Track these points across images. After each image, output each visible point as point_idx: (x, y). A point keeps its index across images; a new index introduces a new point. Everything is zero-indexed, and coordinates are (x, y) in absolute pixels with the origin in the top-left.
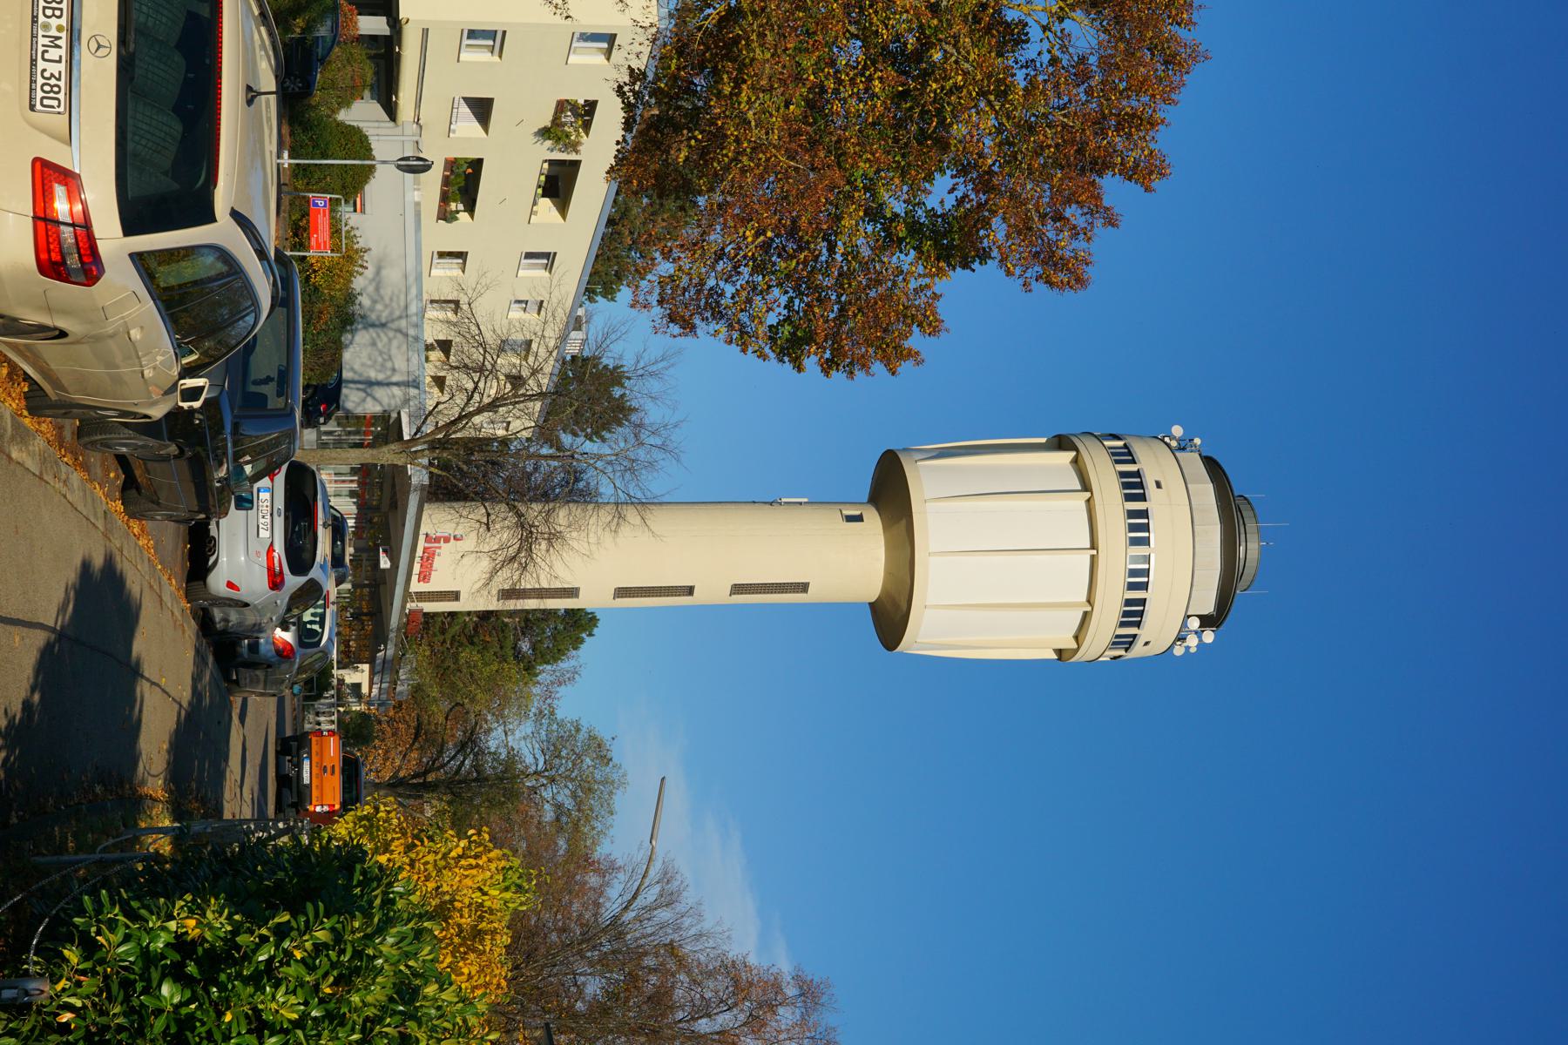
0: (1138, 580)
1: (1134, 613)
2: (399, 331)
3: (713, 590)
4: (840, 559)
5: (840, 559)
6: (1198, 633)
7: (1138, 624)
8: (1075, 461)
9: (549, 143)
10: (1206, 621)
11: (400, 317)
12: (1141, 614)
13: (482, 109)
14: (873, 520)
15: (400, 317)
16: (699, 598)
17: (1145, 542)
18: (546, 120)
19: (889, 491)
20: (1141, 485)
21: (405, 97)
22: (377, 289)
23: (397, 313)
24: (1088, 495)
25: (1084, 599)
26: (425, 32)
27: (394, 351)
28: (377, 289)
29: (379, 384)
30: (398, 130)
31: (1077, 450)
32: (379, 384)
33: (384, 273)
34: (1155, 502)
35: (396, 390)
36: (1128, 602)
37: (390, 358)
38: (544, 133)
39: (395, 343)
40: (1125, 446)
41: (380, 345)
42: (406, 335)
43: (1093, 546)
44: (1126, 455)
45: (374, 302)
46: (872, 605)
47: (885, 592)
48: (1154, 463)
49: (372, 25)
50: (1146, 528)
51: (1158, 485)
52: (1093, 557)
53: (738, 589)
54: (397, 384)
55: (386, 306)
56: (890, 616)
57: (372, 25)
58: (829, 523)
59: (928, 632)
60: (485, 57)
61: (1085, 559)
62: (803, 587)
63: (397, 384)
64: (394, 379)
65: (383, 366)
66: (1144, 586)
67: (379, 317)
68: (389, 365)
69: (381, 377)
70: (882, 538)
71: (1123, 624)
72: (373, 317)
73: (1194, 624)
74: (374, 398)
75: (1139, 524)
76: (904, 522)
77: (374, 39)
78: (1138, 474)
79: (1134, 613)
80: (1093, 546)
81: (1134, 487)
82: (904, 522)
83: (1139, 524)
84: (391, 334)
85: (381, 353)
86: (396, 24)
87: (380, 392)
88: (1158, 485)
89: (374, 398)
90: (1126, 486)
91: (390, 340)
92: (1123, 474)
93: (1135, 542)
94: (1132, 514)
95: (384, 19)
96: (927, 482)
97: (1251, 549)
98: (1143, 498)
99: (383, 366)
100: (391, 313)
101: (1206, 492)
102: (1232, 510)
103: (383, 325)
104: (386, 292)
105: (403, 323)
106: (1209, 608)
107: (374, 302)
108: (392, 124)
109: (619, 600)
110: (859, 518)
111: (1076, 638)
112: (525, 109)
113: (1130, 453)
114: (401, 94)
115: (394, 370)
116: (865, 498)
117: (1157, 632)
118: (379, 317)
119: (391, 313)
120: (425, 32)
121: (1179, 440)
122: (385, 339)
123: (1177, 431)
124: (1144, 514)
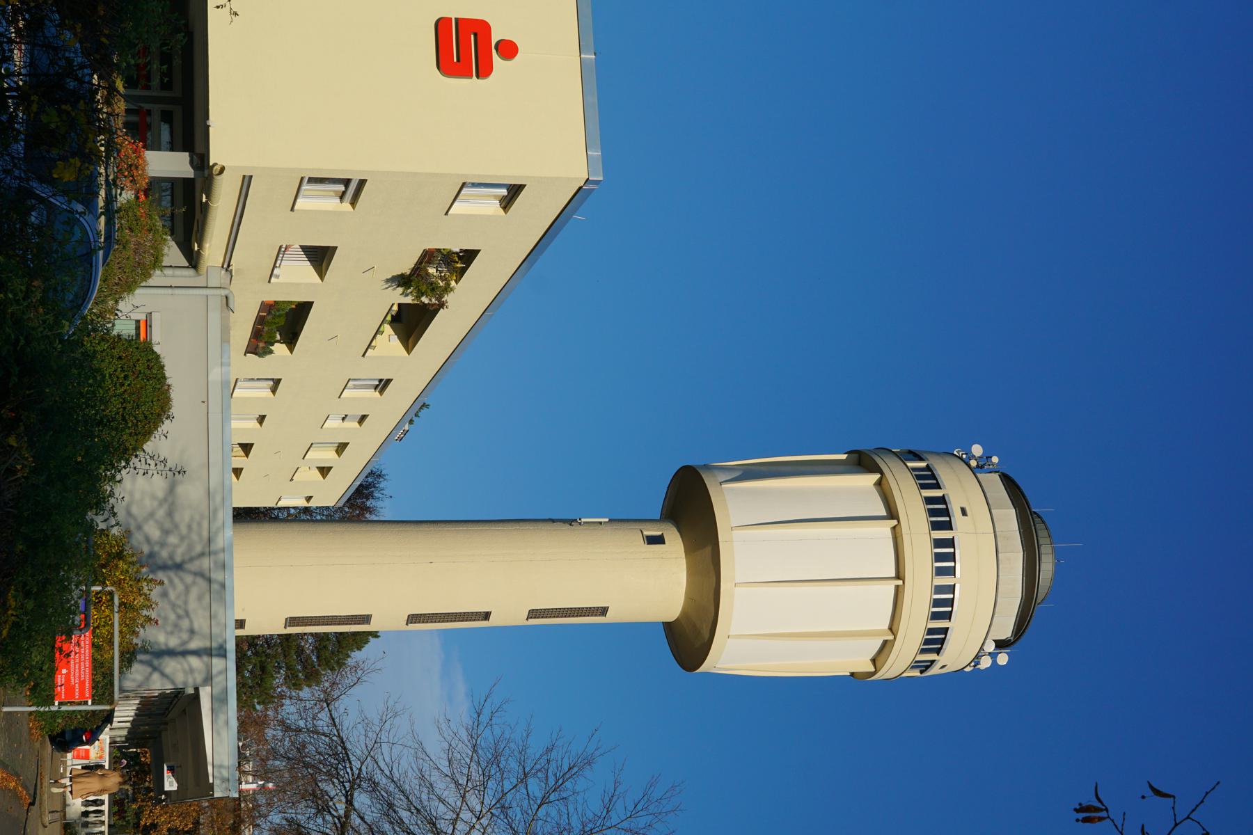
0: (943, 607)
1: (935, 641)
2: (200, 574)
3: (509, 611)
4: (641, 581)
5: (641, 581)
6: (993, 656)
7: (938, 651)
8: (879, 484)
9: (400, 290)
10: (1000, 644)
11: (202, 555)
12: (942, 641)
13: (320, 257)
14: (675, 544)
15: (202, 555)
16: (493, 621)
17: (951, 572)
18: (406, 267)
19: (687, 509)
20: (946, 512)
21: (213, 249)
22: (170, 514)
23: (198, 549)
24: (894, 522)
25: (886, 626)
26: (247, 181)
27: (193, 605)
28: (170, 514)
29: (171, 653)
30: (200, 281)
31: (882, 473)
32: (171, 653)
33: (180, 489)
34: (962, 530)
35: (194, 661)
36: (931, 631)
37: (187, 614)
38: (403, 281)
39: (194, 592)
40: (928, 468)
41: (172, 595)
42: (210, 581)
43: (899, 576)
44: (928, 479)
45: (166, 532)
46: (668, 627)
47: (684, 613)
48: (959, 487)
49: (166, 163)
50: (952, 557)
51: (964, 512)
52: (897, 587)
53: (534, 614)
54: (196, 653)
55: (182, 538)
56: (688, 639)
57: (166, 163)
58: (630, 543)
59: (730, 655)
60: (332, 204)
61: (889, 588)
62: (603, 611)
63: (196, 653)
64: (194, 645)
65: (176, 626)
66: (948, 616)
67: (171, 557)
68: (185, 624)
69: (173, 642)
70: (684, 561)
71: (923, 651)
72: (164, 554)
73: (990, 647)
74: (163, 675)
75: (945, 553)
76: (708, 549)
77: (174, 184)
78: (942, 500)
79: (935, 641)
80: (899, 576)
81: (940, 514)
82: (708, 549)
83: (945, 553)
84: (189, 579)
85: (174, 606)
86: (201, 161)
87: (171, 666)
88: (964, 512)
89: (163, 675)
90: (932, 513)
91: (187, 589)
92: (929, 500)
93: (940, 572)
94: (938, 543)
95: (187, 154)
96: (733, 504)
97: (1047, 568)
98: (948, 526)
99: (176, 626)
100: (190, 547)
101: (1008, 517)
102: (1030, 525)
103: (179, 567)
104: (183, 517)
105: (205, 563)
106: (1006, 632)
107: (166, 532)
108: (191, 272)
109: (659, 533)
110: (658, 540)
111: (874, 661)
112: (379, 250)
113: (933, 477)
114: (207, 246)
115: (192, 632)
116: (655, 506)
117: (955, 656)
118: (171, 557)
119: (190, 547)
120: (247, 181)
121: (978, 459)
122: (180, 587)
123: (977, 450)
124: (950, 543)
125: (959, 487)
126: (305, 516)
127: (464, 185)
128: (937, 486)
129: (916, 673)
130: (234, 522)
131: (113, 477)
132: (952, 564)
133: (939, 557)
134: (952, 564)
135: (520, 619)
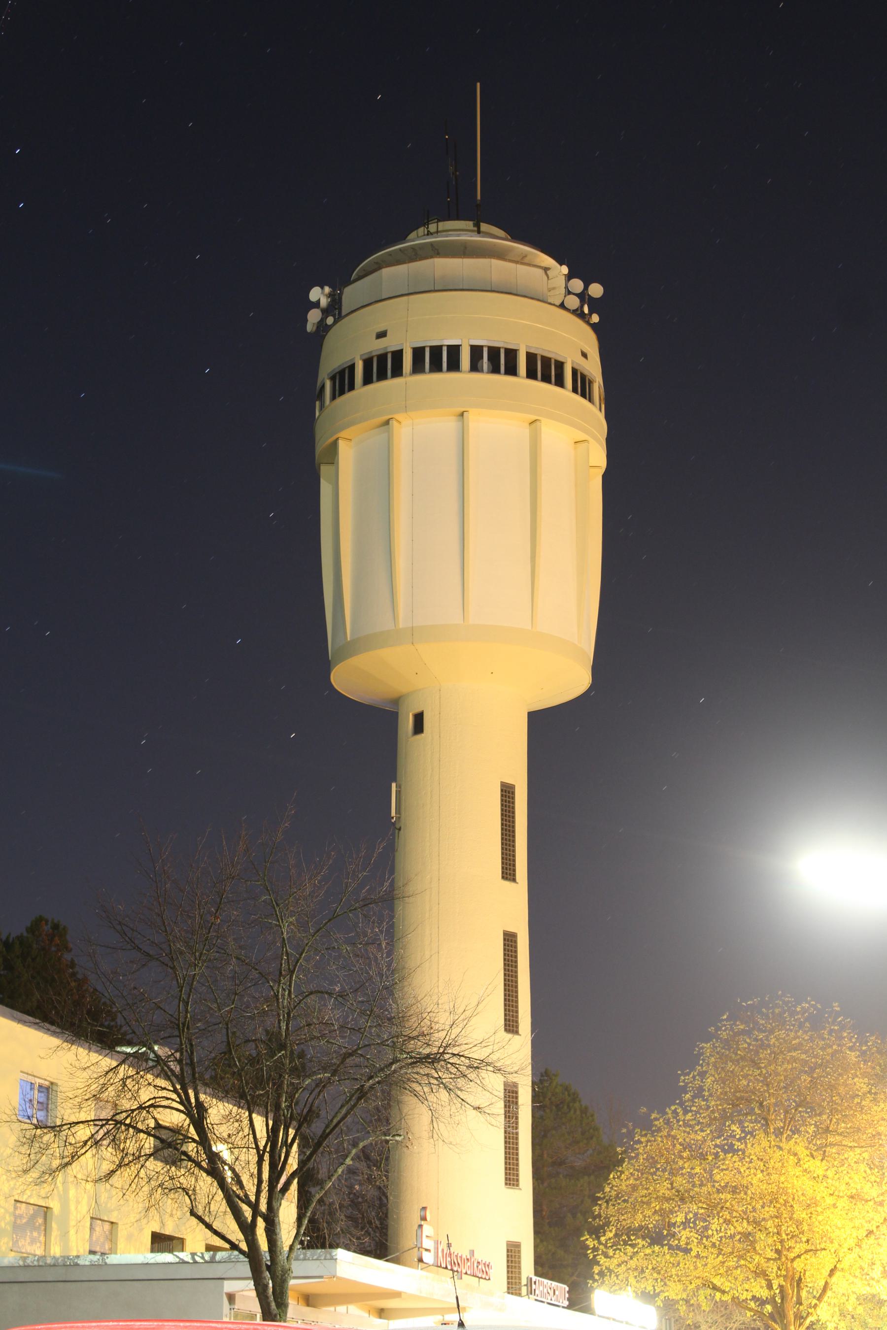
20: (382, 358)
36: (560, 365)
51: (382, 335)
88: (382, 335)
90: (382, 376)
98: (398, 355)
113: (342, 373)
117: (575, 343)
125: (350, 344)
127: (193, 1213)
128: (352, 368)
133: (436, 367)
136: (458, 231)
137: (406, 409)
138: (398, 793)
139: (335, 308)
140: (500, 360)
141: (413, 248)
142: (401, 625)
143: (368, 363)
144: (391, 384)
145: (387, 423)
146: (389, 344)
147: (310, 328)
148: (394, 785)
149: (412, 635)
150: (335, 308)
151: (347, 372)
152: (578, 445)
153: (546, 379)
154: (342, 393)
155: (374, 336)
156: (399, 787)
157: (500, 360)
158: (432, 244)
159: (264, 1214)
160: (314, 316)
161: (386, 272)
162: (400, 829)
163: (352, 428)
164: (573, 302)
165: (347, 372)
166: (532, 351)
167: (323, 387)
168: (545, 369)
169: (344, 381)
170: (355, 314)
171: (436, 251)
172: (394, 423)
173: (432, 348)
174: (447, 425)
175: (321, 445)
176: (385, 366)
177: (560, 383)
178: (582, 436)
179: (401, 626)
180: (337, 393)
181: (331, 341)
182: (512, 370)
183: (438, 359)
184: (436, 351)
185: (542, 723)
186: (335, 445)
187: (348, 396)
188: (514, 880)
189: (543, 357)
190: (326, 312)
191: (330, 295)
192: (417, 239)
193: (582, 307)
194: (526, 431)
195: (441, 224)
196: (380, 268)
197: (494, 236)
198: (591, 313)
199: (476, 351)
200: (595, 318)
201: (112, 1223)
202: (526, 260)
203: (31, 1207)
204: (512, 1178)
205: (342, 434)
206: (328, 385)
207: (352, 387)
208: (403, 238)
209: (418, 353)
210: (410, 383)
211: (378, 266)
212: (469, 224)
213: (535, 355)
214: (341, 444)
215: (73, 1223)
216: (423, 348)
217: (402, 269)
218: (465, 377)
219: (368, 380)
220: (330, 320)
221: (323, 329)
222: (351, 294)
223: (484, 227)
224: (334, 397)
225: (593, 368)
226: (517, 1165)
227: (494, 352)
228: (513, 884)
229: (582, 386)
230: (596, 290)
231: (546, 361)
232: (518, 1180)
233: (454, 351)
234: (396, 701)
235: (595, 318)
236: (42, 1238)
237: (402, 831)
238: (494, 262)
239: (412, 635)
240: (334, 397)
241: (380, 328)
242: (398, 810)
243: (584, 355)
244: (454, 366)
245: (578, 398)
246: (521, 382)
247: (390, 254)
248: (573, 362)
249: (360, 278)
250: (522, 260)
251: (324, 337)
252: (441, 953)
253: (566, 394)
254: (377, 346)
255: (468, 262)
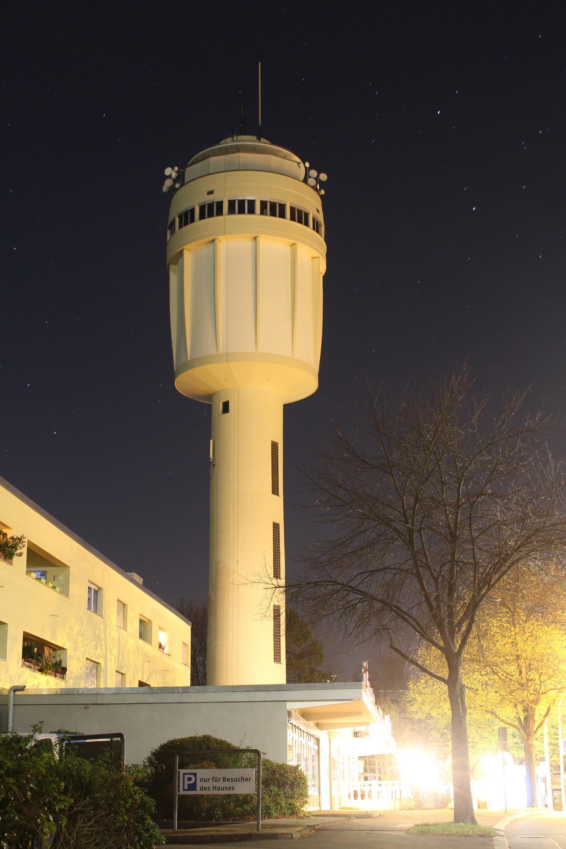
3: (274, 509)
20: (211, 205)
34: (224, 196)
36: (307, 215)
51: (210, 193)
88: (210, 193)
90: (211, 215)
98: (220, 204)
113: (186, 213)
117: (312, 203)
125: (191, 196)
126: (546, 785)
127: (391, 647)
128: (193, 210)
129: (323, 229)
130: (204, 684)
131: (58, 672)
132: (246, 202)
133: (241, 211)
134: (246, 202)
135: (279, 501)
136: (249, 140)
137: (225, 233)
138: (214, 445)
139: (180, 179)
140: (275, 209)
141: (226, 147)
142: (221, 351)
143: (202, 208)
144: (216, 219)
145: (213, 241)
146: (216, 198)
147: (165, 189)
148: (211, 441)
149: (227, 357)
150: (180, 179)
151: (189, 212)
152: (314, 259)
153: (300, 222)
154: (186, 224)
155: (206, 193)
156: (214, 442)
157: (275, 209)
158: (237, 146)
159: (442, 647)
160: (168, 183)
161: (212, 159)
162: (214, 465)
163: (193, 243)
164: (312, 182)
165: (189, 212)
166: (293, 206)
167: (174, 221)
168: (300, 216)
169: (187, 218)
170: (194, 182)
171: (238, 149)
172: (217, 241)
173: (239, 201)
174: (248, 244)
175: (171, 253)
176: (212, 210)
177: (307, 224)
178: (317, 254)
179: (221, 352)
180: (183, 224)
181: (177, 196)
182: (282, 215)
183: (242, 207)
184: (242, 202)
185: (291, 411)
186: (181, 254)
187: (190, 226)
188: (278, 495)
189: (298, 210)
190: (175, 181)
191: (178, 172)
192: (228, 142)
193: (316, 185)
194: (289, 249)
195: (239, 137)
196: (209, 157)
197: (264, 144)
198: (320, 189)
199: (263, 204)
200: (323, 192)
201: (122, 674)
202: (287, 157)
203: (91, 663)
204: (277, 659)
205: (187, 247)
206: (177, 220)
207: (193, 221)
208: (218, 143)
209: (232, 203)
210: (226, 219)
211: (206, 157)
212: (254, 138)
213: (295, 208)
214: (185, 252)
215: (109, 673)
216: (234, 201)
217: (221, 158)
218: (257, 218)
219: (202, 217)
220: (177, 185)
221: (173, 190)
222: (190, 172)
223: (262, 139)
224: (180, 227)
225: (320, 218)
226: (280, 650)
227: (273, 205)
228: (277, 497)
229: (316, 228)
230: (323, 177)
231: (300, 212)
232: (280, 659)
233: (252, 203)
234: (210, 397)
235: (323, 192)
236: (95, 682)
237: (215, 467)
238: (272, 157)
239: (227, 357)
240: (180, 227)
241: (210, 189)
242: (214, 456)
243: (318, 211)
244: (252, 211)
245: (315, 233)
246: (287, 222)
247: (212, 150)
248: (313, 214)
249: (193, 164)
250: (284, 157)
251: (173, 195)
252: (239, 533)
253: (309, 230)
254: (209, 199)
255: (258, 156)
